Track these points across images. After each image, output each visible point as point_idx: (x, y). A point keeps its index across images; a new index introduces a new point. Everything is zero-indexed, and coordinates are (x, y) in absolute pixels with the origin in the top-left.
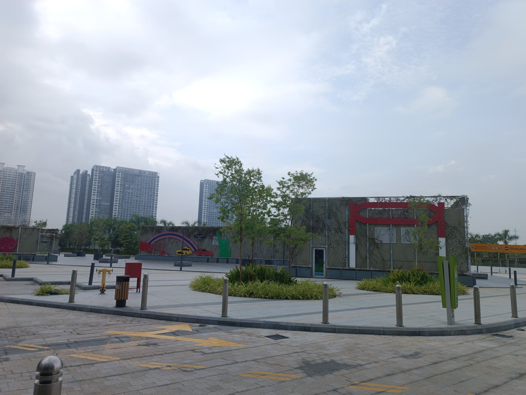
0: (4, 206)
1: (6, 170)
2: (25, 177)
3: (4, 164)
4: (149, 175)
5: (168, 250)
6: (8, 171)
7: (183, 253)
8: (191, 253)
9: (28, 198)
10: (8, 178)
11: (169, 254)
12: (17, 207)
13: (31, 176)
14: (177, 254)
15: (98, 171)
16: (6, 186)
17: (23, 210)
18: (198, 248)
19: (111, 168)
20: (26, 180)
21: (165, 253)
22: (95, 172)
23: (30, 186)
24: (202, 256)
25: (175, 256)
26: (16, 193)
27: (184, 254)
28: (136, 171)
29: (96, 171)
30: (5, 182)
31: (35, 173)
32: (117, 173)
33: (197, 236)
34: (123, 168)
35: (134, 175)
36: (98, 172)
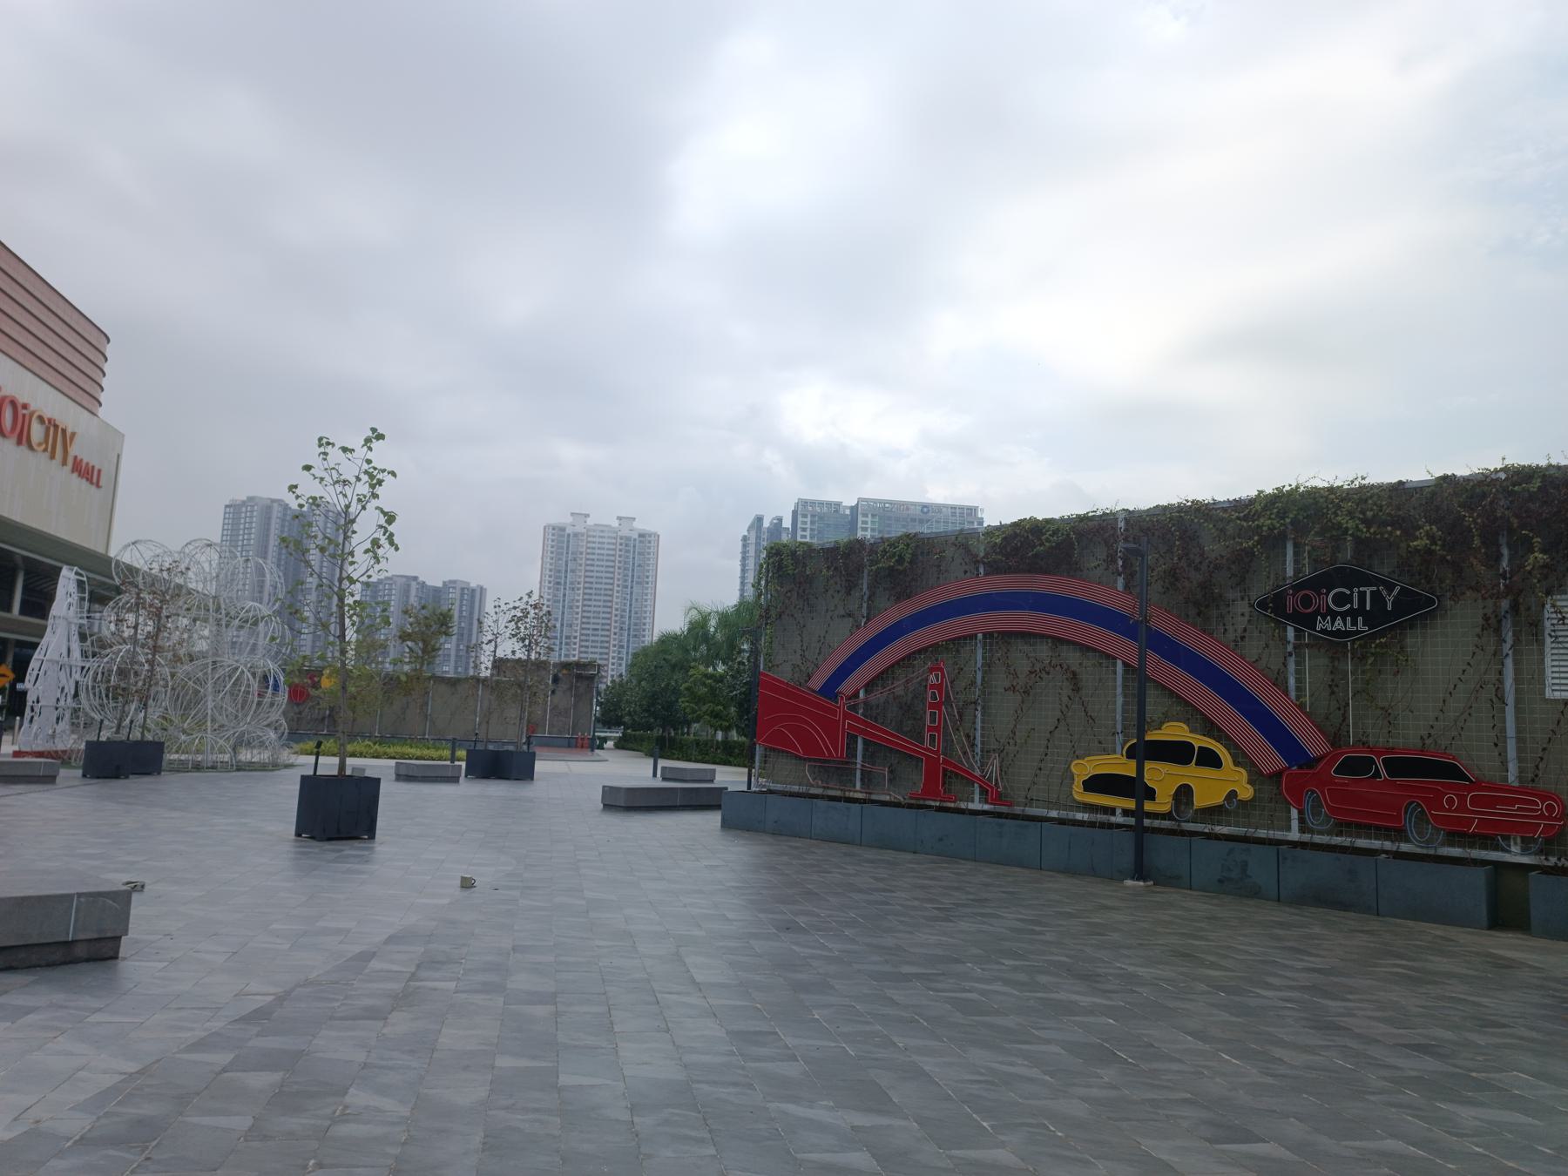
1: (594, 531)
2: (634, 546)
3: (587, 516)
4: (952, 516)
5: (986, 753)
6: (598, 534)
7: (1150, 794)
8: (1246, 792)
9: (645, 597)
10: (599, 551)
11: (998, 798)
12: (621, 629)
13: (650, 542)
14: (1079, 794)
15: (809, 516)
18: (1336, 739)
19: (844, 504)
20: (639, 554)
21: (969, 779)
22: (800, 519)
23: (648, 571)
24: (1400, 834)
25: (1061, 822)
26: (618, 592)
27: (1163, 802)
28: (913, 507)
29: (805, 516)
31: (658, 536)
32: (860, 519)
33: (1307, 601)
34: (875, 501)
35: (909, 520)
36: (809, 520)
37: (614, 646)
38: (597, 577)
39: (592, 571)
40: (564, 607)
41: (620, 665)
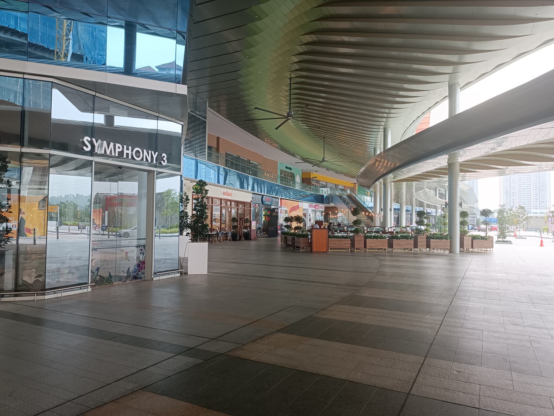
0: (522, 188)
12: (536, 188)
16: (522, 201)
17: (542, 190)
30: (521, 197)
37: (533, 194)
38: (523, 182)
39: (521, 180)
40: (510, 182)
41: (537, 202)
